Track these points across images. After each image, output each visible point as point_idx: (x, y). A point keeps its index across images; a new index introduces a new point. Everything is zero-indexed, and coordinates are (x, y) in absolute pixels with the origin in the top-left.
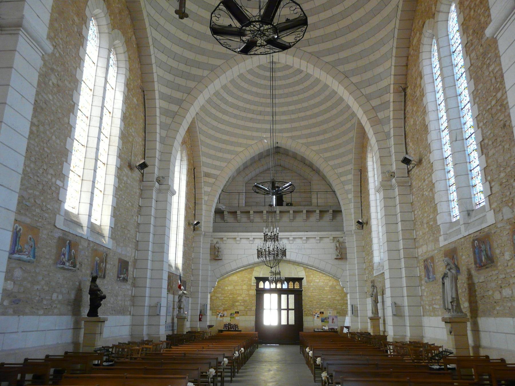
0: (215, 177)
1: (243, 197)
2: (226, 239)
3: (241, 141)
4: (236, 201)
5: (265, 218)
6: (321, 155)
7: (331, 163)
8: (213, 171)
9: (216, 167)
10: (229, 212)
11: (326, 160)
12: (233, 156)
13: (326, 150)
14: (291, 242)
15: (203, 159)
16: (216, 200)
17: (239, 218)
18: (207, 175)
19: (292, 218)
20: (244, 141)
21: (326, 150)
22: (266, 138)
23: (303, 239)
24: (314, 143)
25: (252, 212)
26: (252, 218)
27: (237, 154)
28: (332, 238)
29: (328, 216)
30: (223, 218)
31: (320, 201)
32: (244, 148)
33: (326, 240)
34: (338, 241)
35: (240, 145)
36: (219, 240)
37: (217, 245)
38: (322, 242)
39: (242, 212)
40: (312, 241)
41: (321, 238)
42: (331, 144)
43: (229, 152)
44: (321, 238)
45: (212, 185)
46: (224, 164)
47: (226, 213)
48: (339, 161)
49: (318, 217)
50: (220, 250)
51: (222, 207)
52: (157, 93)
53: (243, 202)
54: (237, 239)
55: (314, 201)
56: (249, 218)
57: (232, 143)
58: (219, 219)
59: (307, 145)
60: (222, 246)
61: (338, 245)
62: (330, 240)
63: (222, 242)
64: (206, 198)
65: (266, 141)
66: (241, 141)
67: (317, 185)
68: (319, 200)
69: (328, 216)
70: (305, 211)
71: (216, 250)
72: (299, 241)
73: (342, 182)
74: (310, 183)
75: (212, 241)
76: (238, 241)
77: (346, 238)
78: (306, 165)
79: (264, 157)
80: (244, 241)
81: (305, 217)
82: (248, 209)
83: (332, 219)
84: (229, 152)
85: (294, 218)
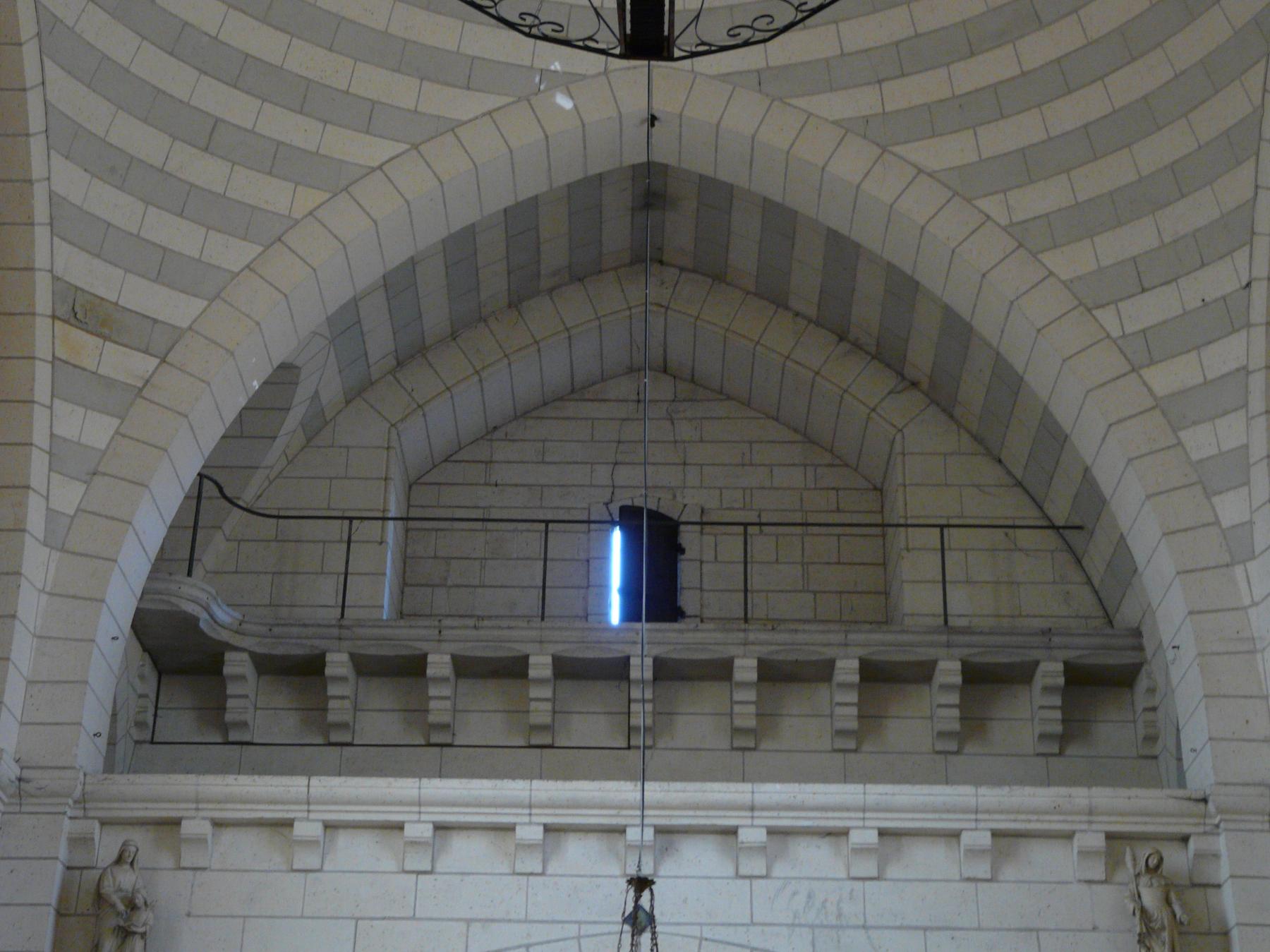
0: (161, 342)
1: (382, 557)
2: (207, 828)
3: (373, 82)
4: (327, 591)
5: (541, 713)
6: (989, 205)
7: (1071, 261)
8: (140, 295)
9: (164, 267)
10: (267, 666)
11: (1027, 238)
12: (309, 198)
13: (1027, 166)
14: (755, 865)
15: (58, 177)
16: (152, 523)
17: (337, 711)
18: (83, 312)
19: (746, 717)
20: (400, 91)
21: (1027, 166)
22: (568, 82)
23: (856, 837)
24: (931, 120)
25: (439, 664)
26: (439, 711)
27: (342, 181)
28: (1098, 841)
29: (1029, 714)
30: (213, 711)
31: (960, 601)
32: (408, 147)
33: (1047, 860)
34: (1154, 869)
35: (369, 115)
36: (138, 837)
37: (126, 879)
38: (1009, 872)
39: (366, 667)
40: (927, 859)
41: (1007, 840)
42: (1069, 114)
43: (277, 160)
44: (1007, 840)
45: (123, 398)
46: (232, 253)
47: (236, 664)
48: (1138, 238)
49: (950, 718)
50: (144, 918)
51: (209, 604)
52: (43, 285)
53: (378, 594)
54: (300, 830)
55: (918, 599)
56: (416, 712)
57: (304, 96)
58: (180, 722)
59: (880, 133)
60: (165, 885)
61: (1150, 898)
62: (1084, 854)
63: (166, 861)
64: (68, 495)
65: (565, 102)
66: (373, 82)
67: (930, 472)
68: (952, 588)
69: (1029, 714)
70: (848, 669)
71: (111, 921)
72: (814, 858)
73: (1160, 405)
74: (879, 490)
75: (80, 842)
76: (310, 843)
77: (1221, 843)
78: (857, 345)
79: (551, 291)
80: (355, 851)
81: (848, 716)
82: (411, 637)
83: (1064, 739)
84: (277, 160)
85: (767, 718)
